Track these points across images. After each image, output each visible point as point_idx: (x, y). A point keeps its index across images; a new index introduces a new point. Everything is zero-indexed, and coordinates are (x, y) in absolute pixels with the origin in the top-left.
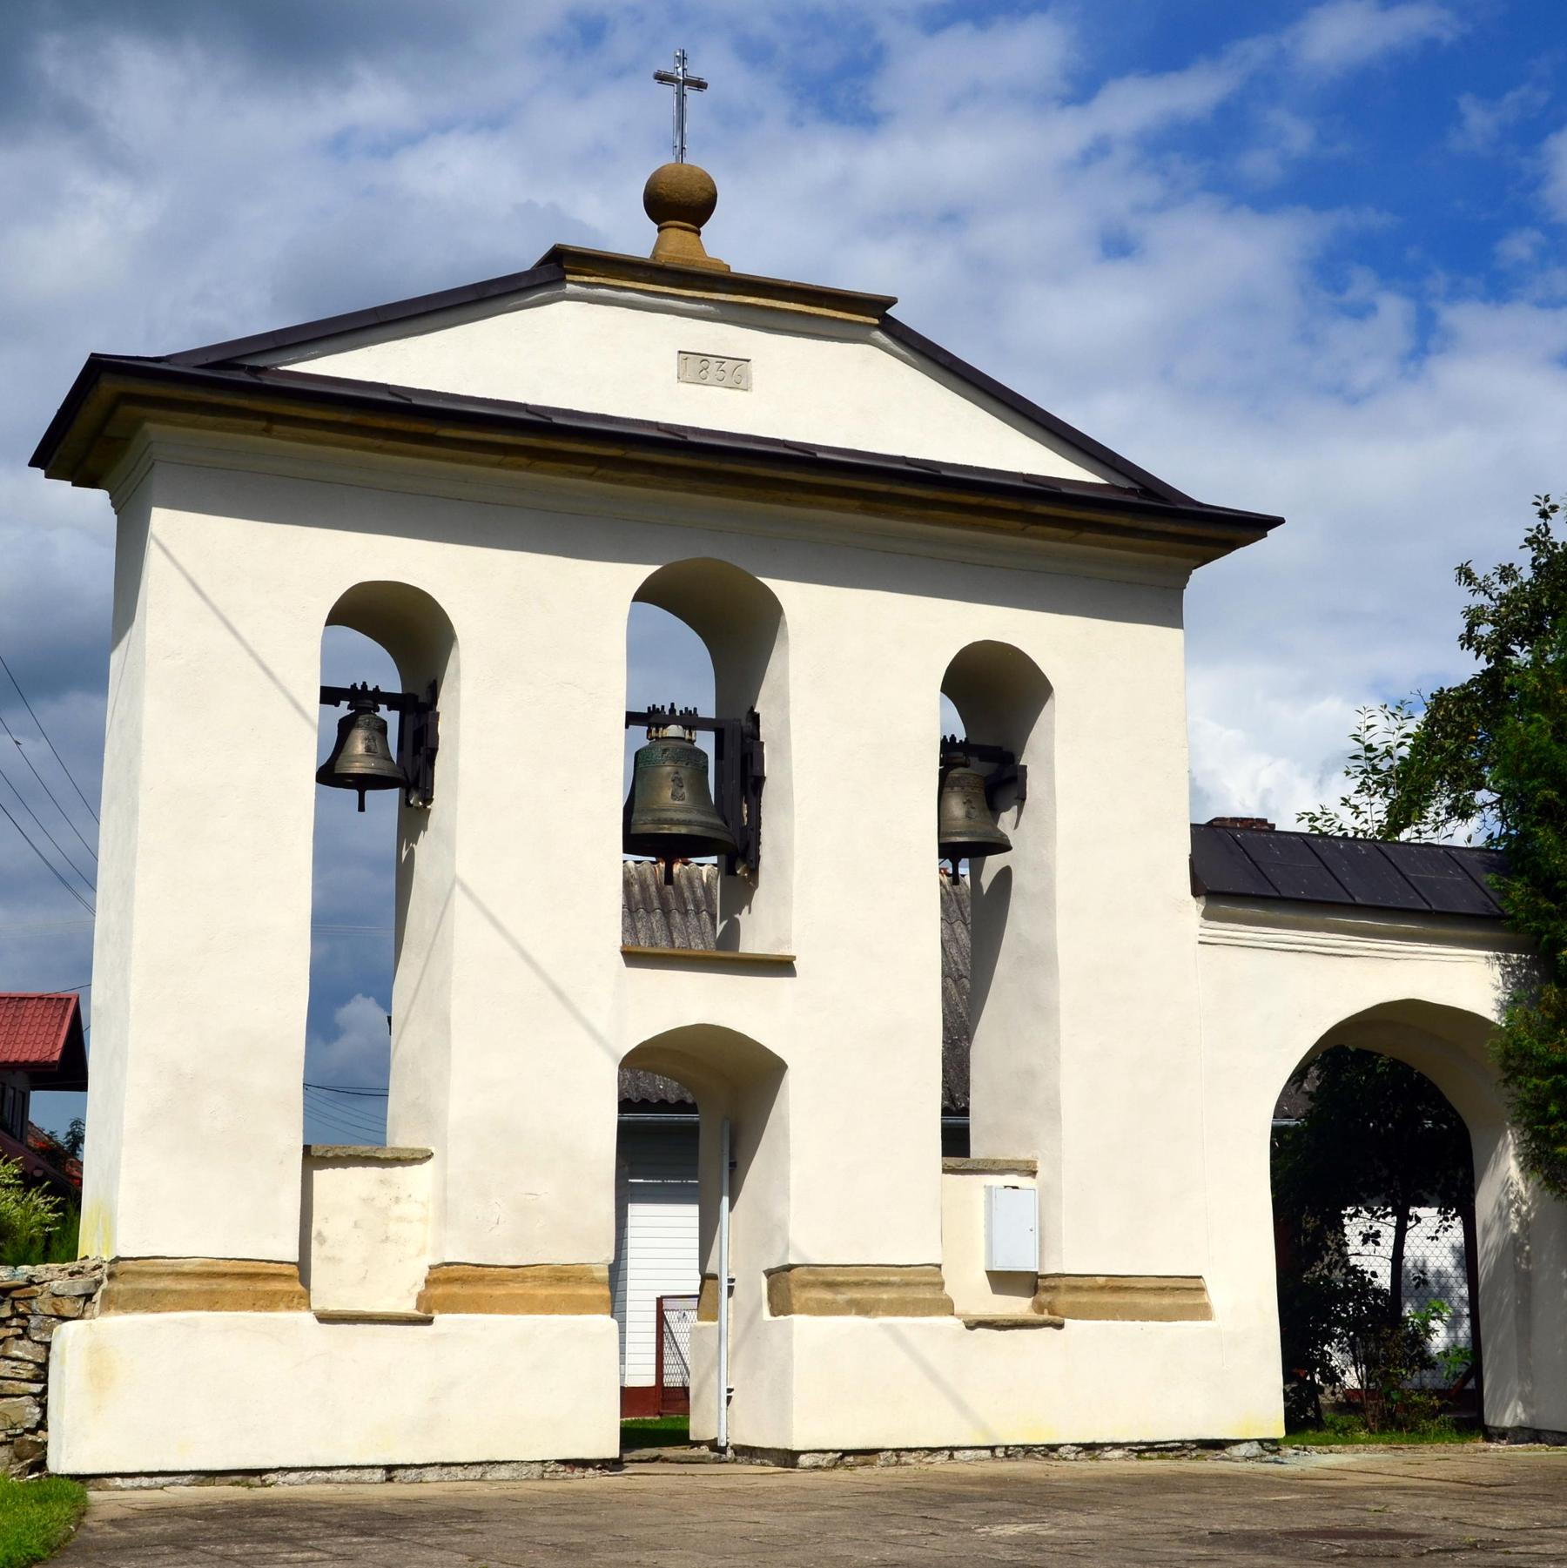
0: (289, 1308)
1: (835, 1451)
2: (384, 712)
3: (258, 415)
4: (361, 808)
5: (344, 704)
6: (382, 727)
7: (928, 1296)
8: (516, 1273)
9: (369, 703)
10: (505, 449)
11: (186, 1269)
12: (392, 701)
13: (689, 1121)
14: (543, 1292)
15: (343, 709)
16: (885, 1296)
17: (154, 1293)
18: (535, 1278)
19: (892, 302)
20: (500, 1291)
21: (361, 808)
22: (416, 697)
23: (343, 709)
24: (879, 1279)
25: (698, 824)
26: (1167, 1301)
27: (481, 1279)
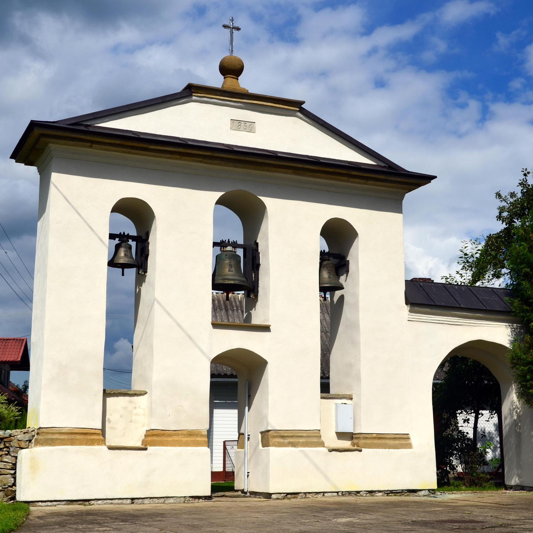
0: (98, 445)
1: (284, 493)
2: (130, 242)
3: (88, 141)
4: (123, 275)
5: (117, 239)
6: (130, 247)
7: (316, 440)
8: (176, 433)
9: (125, 239)
10: (172, 153)
11: (63, 431)
12: (133, 238)
13: (234, 381)
14: (185, 439)
15: (117, 241)
16: (301, 441)
17: (52, 439)
18: (182, 434)
19: (303, 103)
20: (170, 439)
21: (123, 275)
22: (141, 237)
23: (117, 241)
24: (299, 435)
25: (237, 280)
26: (397, 442)
27: (164, 435)
